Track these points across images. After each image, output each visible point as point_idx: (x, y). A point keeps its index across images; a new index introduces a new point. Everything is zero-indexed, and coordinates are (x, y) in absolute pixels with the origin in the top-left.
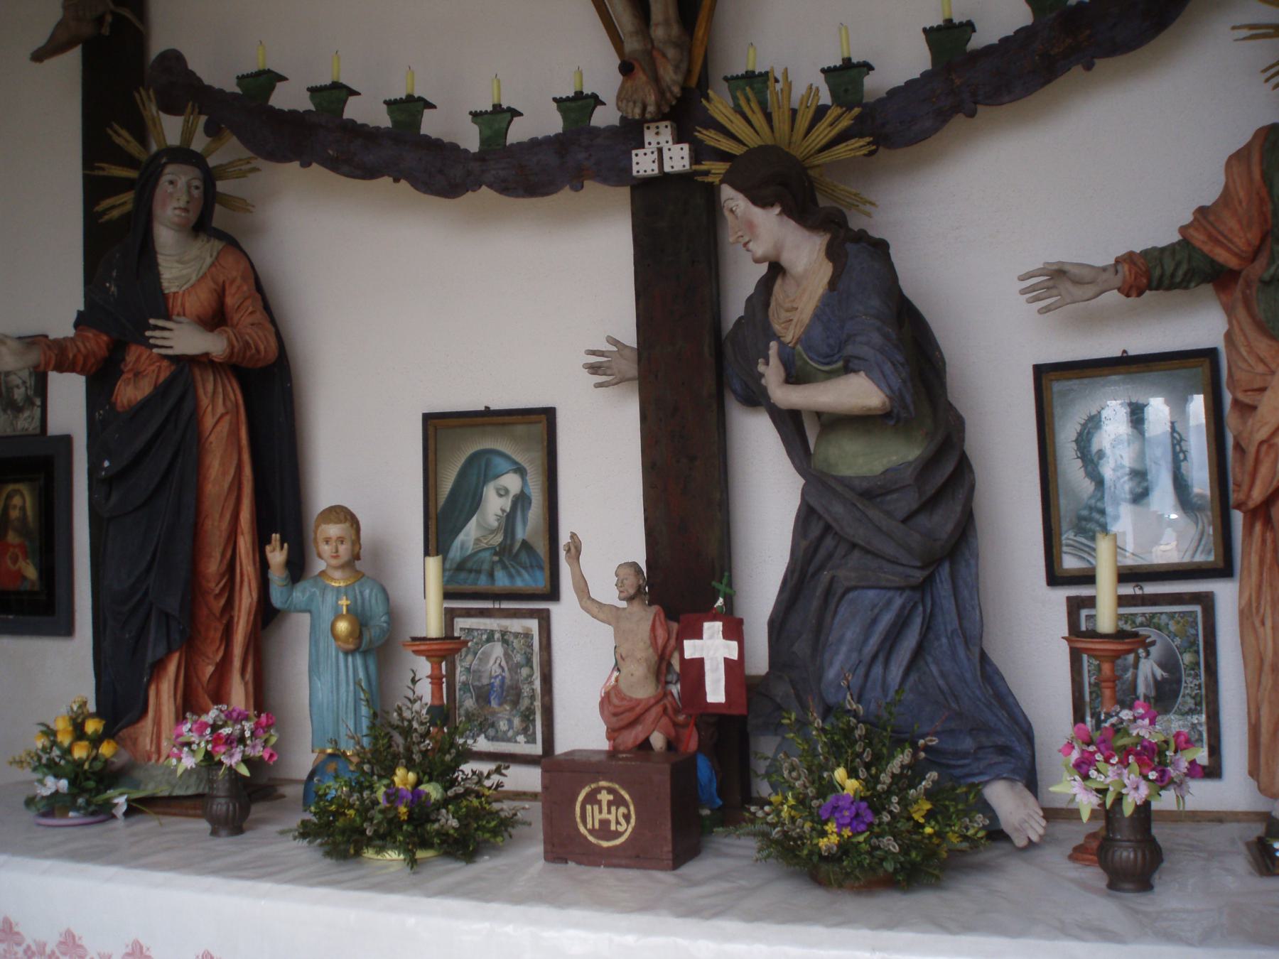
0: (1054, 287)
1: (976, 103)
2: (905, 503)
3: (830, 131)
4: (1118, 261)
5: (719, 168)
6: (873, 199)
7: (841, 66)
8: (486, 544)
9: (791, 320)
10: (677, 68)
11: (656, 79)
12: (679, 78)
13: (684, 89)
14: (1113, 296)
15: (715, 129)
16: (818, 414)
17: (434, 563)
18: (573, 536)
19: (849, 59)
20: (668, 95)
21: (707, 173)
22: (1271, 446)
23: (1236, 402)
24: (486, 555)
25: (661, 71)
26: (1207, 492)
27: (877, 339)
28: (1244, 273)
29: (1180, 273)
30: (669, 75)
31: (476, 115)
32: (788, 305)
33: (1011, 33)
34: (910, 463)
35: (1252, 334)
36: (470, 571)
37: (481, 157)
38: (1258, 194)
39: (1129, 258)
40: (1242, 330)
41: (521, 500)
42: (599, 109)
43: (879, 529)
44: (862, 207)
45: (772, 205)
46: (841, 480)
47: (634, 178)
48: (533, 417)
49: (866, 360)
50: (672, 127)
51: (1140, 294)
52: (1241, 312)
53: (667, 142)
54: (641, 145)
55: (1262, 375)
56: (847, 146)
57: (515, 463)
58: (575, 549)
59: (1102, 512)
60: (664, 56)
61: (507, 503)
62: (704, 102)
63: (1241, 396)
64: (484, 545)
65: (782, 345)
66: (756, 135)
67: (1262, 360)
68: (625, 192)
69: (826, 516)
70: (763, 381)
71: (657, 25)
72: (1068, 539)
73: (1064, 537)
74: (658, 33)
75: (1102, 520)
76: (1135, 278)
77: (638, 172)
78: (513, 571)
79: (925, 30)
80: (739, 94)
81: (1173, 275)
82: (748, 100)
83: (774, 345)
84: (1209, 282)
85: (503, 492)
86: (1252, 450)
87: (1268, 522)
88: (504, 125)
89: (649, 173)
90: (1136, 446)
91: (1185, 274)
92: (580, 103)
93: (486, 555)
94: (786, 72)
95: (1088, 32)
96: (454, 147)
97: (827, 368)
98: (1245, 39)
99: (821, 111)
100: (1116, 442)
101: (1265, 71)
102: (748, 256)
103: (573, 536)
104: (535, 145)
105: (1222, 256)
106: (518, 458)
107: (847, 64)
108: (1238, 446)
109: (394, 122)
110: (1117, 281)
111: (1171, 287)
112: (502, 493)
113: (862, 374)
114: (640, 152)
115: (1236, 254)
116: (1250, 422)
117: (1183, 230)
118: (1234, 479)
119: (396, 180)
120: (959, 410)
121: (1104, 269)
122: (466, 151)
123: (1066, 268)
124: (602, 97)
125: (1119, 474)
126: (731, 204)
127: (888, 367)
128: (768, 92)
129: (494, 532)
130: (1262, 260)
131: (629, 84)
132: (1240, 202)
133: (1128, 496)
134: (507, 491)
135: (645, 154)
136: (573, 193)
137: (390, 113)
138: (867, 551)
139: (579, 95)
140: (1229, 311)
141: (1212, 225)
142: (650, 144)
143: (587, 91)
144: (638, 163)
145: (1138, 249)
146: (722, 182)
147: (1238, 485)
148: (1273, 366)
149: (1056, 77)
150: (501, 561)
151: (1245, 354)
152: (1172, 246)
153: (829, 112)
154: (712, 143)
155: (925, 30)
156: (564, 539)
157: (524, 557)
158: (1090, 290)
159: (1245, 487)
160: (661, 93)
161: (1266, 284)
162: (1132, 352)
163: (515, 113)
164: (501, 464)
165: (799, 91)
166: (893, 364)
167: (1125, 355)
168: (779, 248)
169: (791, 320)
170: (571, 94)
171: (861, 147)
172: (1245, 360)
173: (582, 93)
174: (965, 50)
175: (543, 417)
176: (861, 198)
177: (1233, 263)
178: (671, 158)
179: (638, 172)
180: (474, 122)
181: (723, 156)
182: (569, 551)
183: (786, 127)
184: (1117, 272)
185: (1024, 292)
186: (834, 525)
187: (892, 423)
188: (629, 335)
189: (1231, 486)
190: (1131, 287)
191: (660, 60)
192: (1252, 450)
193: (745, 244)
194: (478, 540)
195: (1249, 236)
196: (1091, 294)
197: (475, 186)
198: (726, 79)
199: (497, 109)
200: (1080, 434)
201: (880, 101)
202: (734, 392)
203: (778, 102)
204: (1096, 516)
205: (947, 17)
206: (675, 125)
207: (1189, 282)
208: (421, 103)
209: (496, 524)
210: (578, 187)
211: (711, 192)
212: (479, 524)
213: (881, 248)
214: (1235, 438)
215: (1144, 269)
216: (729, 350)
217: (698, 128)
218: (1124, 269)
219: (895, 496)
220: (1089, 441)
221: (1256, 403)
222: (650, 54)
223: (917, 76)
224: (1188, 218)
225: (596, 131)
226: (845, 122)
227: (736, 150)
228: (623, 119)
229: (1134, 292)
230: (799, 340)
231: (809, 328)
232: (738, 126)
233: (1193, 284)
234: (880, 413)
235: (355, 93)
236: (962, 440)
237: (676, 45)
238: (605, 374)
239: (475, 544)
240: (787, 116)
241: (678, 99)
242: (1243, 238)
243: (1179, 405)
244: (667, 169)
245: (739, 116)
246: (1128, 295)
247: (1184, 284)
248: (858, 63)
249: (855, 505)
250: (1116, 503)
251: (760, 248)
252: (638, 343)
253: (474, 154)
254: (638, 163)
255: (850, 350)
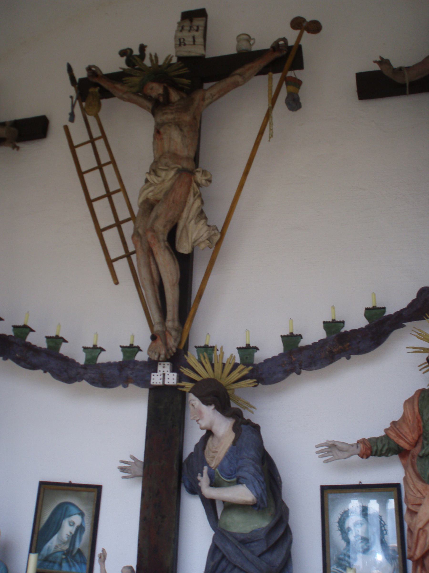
0: (331, 452)
1: (301, 369)
2: (260, 547)
3: (238, 375)
4: (358, 442)
5: (189, 385)
6: (254, 405)
7: (245, 347)
8: (60, 549)
9: (214, 457)
10: (175, 340)
11: (166, 344)
12: (176, 344)
13: (177, 349)
14: (356, 458)
15: (189, 368)
16: (224, 502)
17: (33, 557)
18: (103, 550)
19: (249, 345)
20: (170, 351)
21: (183, 387)
22: (424, 531)
23: (408, 509)
24: (59, 554)
25: (168, 340)
26: (396, 545)
27: (252, 469)
28: (411, 452)
29: (385, 449)
30: (172, 343)
31: (85, 348)
32: (214, 450)
33: (317, 341)
34: (264, 528)
35: (415, 479)
36: (51, 562)
37: (85, 367)
38: (417, 418)
39: (363, 441)
40: (411, 477)
41: (80, 529)
42: (140, 353)
43: (247, 559)
44: (250, 408)
45: (211, 405)
46: (231, 534)
47: (151, 385)
48: (91, 489)
49: (246, 479)
50: (170, 365)
51: (367, 457)
52: (410, 470)
53: (168, 371)
54: (156, 371)
55: (420, 498)
56: (245, 382)
57: (80, 510)
58: (103, 557)
59: (349, 557)
60: (170, 334)
61: (73, 530)
62: (185, 356)
63: (411, 507)
64: (59, 549)
65: (209, 468)
66: (206, 373)
67: (419, 491)
68: (146, 391)
69: (223, 551)
70: (200, 484)
71: (169, 321)
72: (333, 569)
73: (332, 568)
74: (169, 324)
75: (349, 560)
76: (366, 450)
77: (153, 383)
78: (71, 564)
79: (282, 336)
80: (201, 355)
81: (381, 450)
82: (204, 358)
83: (206, 468)
84: (396, 454)
85: (72, 524)
86: (416, 532)
87: (423, 567)
88: (97, 354)
89: (158, 384)
90: (364, 526)
91: (387, 450)
92: (131, 349)
93: (59, 554)
94: (222, 348)
95: (348, 344)
96: (73, 361)
97: (229, 481)
98: (411, 352)
99: (236, 366)
100: (356, 524)
101: (419, 366)
102: (198, 426)
103: (103, 550)
104: (109, 365)
105: (403, 444)
106: (82, 508)
107: (248, 347)
108: (409, 530)
109: (49, 347)
110: (358, 451)
111: (381, 455)
112: (72, 524)
113: (245, 485)
114: (155, 374)
115: (408, 443)
116: (415, 519)
117: (386, 430)
118: (408, 546)
119: (45, 372)
120: (286, 504)
121: (352, 445)
122: (78, 364)
123: (337, 444)
124: (141, 348)
125: (357, 539)
126: (193, 402)
127: (256, 483)
128: (213, 355)
129: (65, 543)
130: (419, 447)
131: (154, 344)
132: (410, 421)
133: (361, 550)
134: (74, 524)
135: (157, 375)
136: (123, 388)
137: (48, 342)
138: (241, 570)
139: (131, 346)
140: (405, 467)
141: (397, 429)
142: (160, 371)
143: (135, 344)
144: (153, 379)
145: (367, 438)
146: (190, 392)
147: (410, 548)
148: (424, 494)
149: (335, 361)
150: (66, 558)
151: (412, 488)
152: (382, 437)
153: (239, 367)
154: (187, 374)
155: (282, 336)
156: (98, 551)
157: (78, 557)
158: (346, 454)
159: (413, 550)
160: (167, 350)
161: (421, 457)
162: (364, 483)
163: (102, 350)
164: (73, 510)
165: (227, 356)
166: (259, 482)
167: (360, 484)
168: (212, 424)
169: (214, 457)
170: (128, 345)
171: (251, 383)
172: (412, 491)
173: (132, 345)
174: (297, 346)
175: (96, 490)
176: (249, 405)
177: (406, 446)
178: (168, 378)
179: (154, 375)
180: (84, 351)
181: (191, 380)
182: (100, 558)
183: (220, 371)
184: (358, 447)
185: (317, 452)
186: (227, 555)
187: (256, 509)
188: (141, 456)
189: (407, 549)
190: (363, 455)
191: (168, 336)
192: (416, 532)
193: (197, 421)
194: (56, 547)
195: (414, 436)
196: (346, 456)
197: (80, 379)
198: (196, 347)
199: (95, 347)
200: (340, 519)
201: (260, 364)
202: (186, 487)
203: (217, 361)
204: (347, 558)
205: (291, 331)
206: (172, 364)
207: (389, 453)
208: (62, 340)
209: (66, 539)
210: (125, 386)
211: (184, 395)
212: (58, 539)
213: (256, 428)
214: (408, 526)
215: (369, 446)
216: (185, 467)
217: (182, 367)
218: (361, 446)
219: (256, 544)
220: (344, 523)
221: (417, 511)
222: (165, 332)
223: (277, 354)
224: (388, 426)
225: (136, 363)
226: (245, 372)
227: (198, 379)
228: (149, 359)
229: (365, 456)
230: (217, 467)
231: (221, 463)
232: (199, 368)
233: (390, 455)
234: (252, 504)
235: (32, 331)
236: (287, 519)
237: (176, 330)
238: (127, 473)
239: (55, 548)
240: (221, 365)
241: (174, 353)
242: (411, 436)
243: (383, 504)
244: (166, 383)
245: (200, 364)
246: (362, 458)
247: (386, 454)
248: (253, 347)
249: (237, 547)
250: (356, 553)
251: (204, 423)
252: (145, 460)
253: (82, 365)
254: (153, 379)
255: (240, 473)
